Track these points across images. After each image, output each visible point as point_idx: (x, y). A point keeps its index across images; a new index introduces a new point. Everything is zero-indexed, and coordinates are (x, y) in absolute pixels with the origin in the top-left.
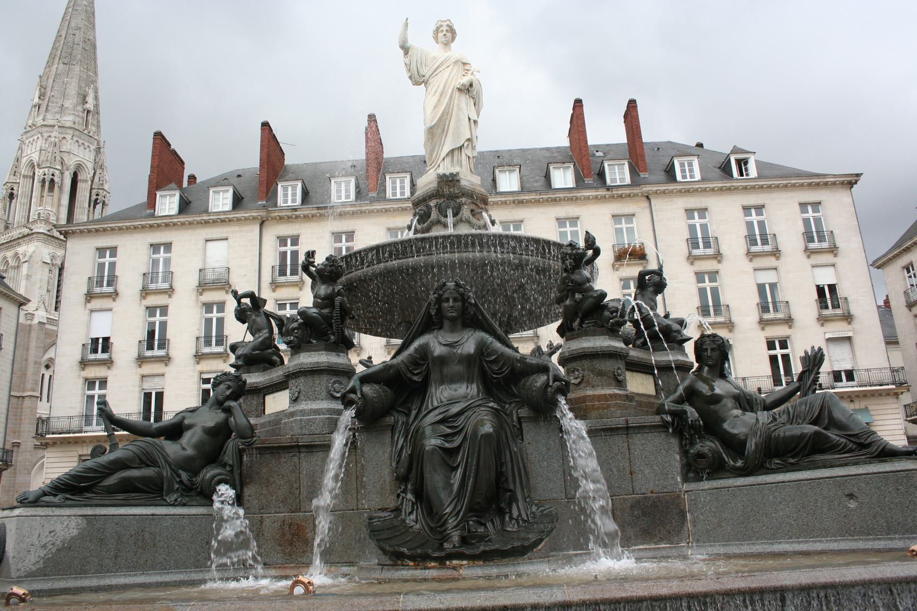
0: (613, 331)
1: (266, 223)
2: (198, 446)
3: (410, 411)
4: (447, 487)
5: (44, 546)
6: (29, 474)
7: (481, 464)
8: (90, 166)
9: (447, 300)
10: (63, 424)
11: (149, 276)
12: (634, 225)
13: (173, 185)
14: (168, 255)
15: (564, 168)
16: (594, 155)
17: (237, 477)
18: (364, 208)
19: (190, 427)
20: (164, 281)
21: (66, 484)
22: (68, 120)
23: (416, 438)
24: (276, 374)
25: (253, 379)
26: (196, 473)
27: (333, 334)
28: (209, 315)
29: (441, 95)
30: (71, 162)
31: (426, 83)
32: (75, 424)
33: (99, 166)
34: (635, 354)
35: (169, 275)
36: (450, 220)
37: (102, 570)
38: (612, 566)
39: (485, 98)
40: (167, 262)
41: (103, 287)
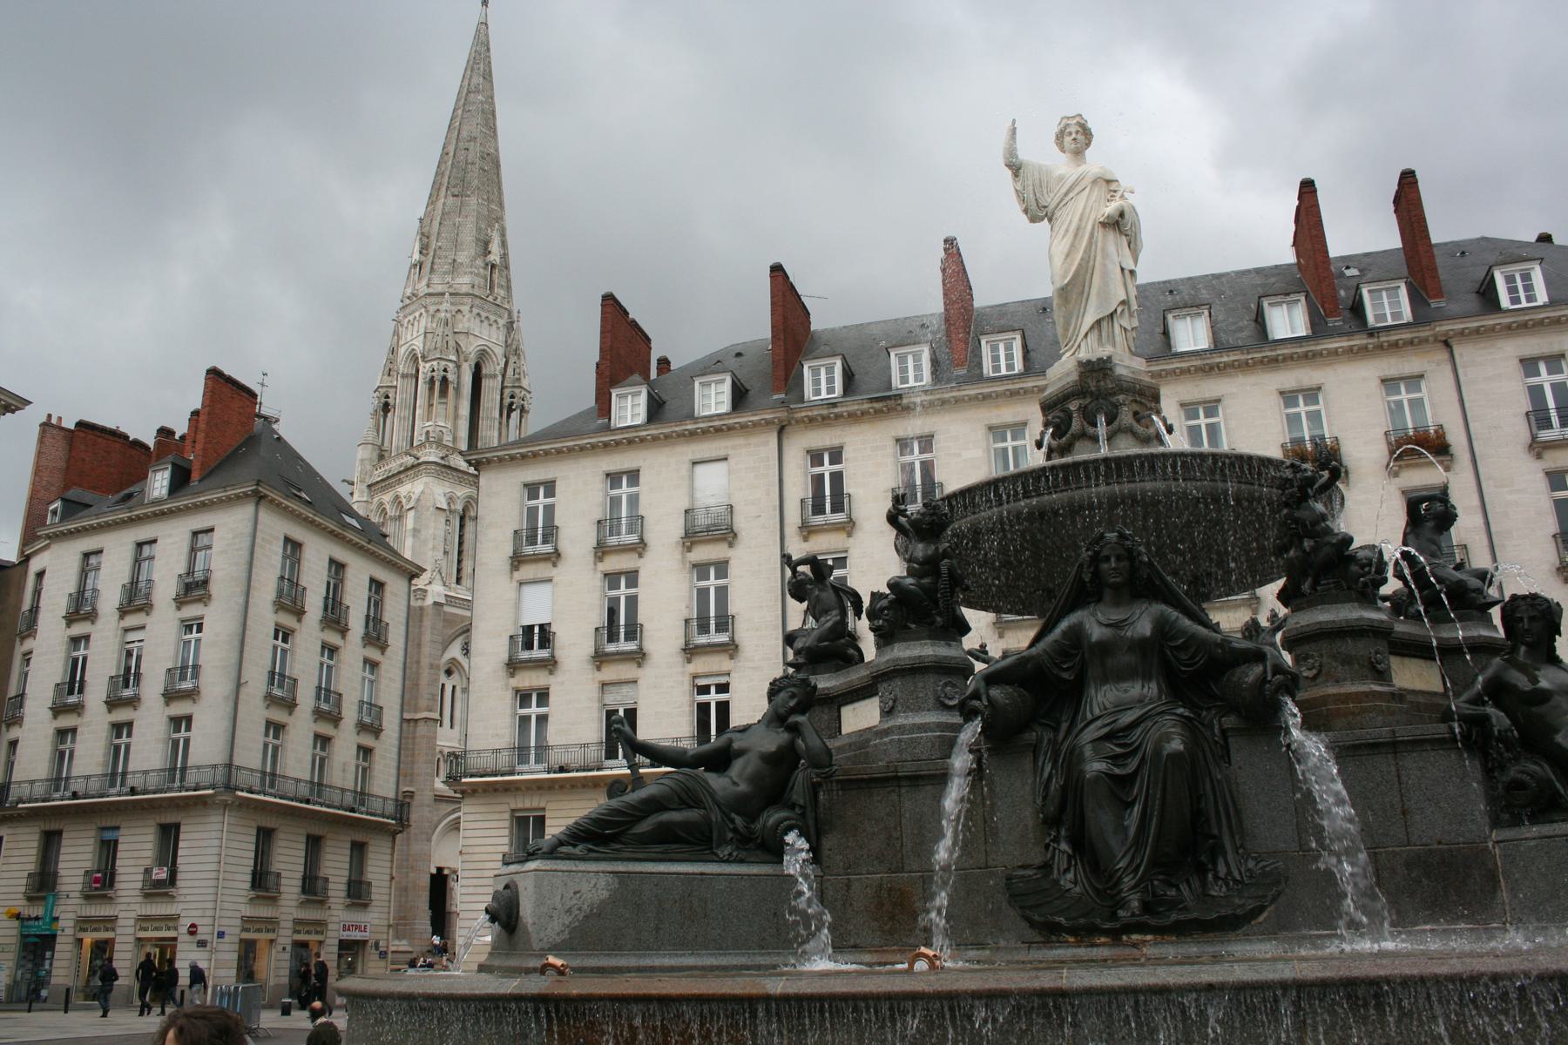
0: (1367, 594)
1: (788, 429)
2: (754, 780)
3: (1059, 724)
4: (1119, 832)
5: (569, 911)
6: (429, 840)
8: (499, 351)
9: (1107, 559)
10: (486, 762)
11: (606, 525)
12: (1424, 393)
13: (636, 377)
14: (634, 489)
15: (1288, 303)
16: (1342, 275)
17: (811, 822)
18: (947, 396)
19: (741, 753)
20: (630, 532)
21: (586, 831)
22: (463, 282)
23: (1072, 761)
24: (856, 676)
25: (825, 682)
26: (752, 817)
27: (940, 614)
28: (703, 584)
29: (1076, 235)
30: (471, 347)
32: (504, 761)
33: (513, 350)
34: (1402, 627)
35: (637, 522)
36: (1102, 430)
37: (640, 946)
38: (1375, 946)
40: (634, 500)
41: (535, 547)
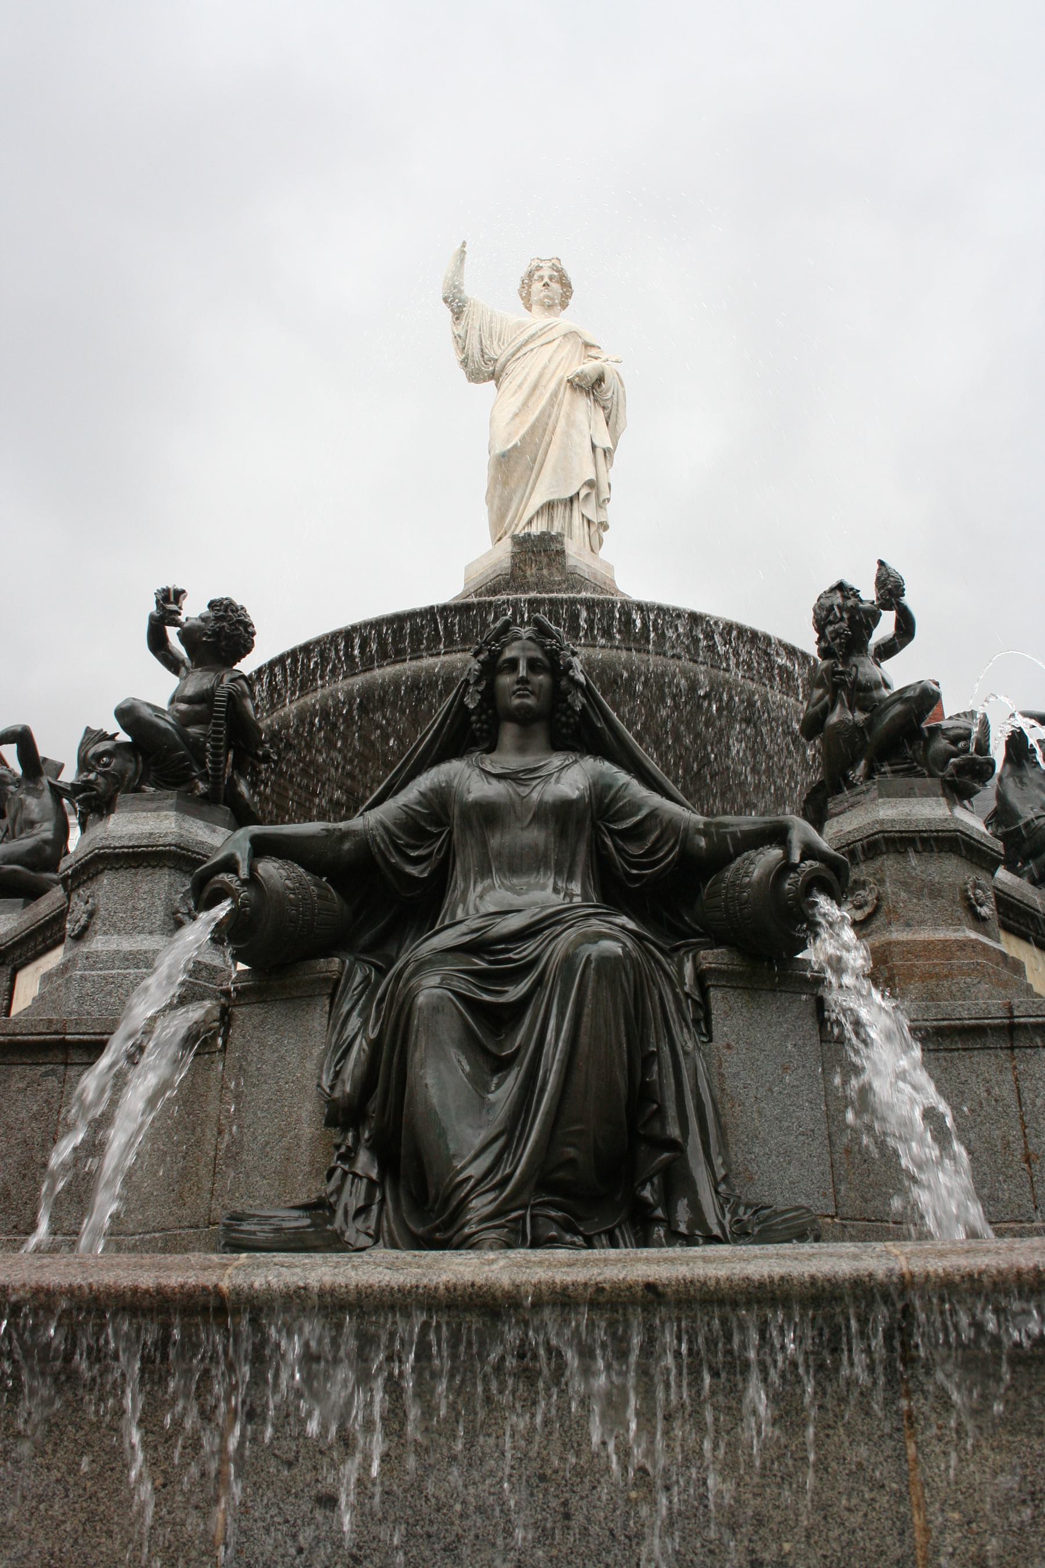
7: (584, 1040)
27: (204, 777)
31: (495, 376)
39: (632, 413)
